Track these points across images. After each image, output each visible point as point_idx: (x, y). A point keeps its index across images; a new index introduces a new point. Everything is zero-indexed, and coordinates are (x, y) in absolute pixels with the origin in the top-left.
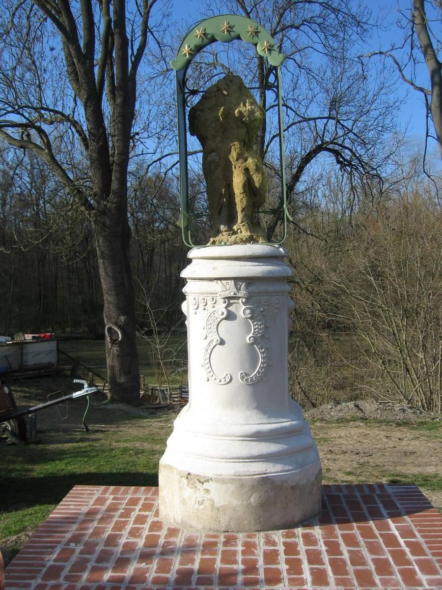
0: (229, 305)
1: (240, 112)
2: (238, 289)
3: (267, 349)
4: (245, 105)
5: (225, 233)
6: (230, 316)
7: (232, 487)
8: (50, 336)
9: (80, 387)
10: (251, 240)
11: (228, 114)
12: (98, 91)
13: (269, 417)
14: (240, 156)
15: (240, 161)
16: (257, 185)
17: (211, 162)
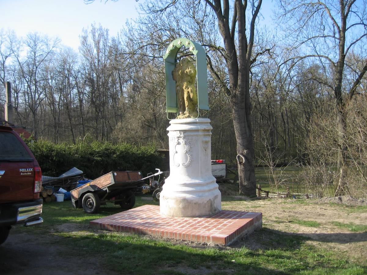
0: (179, 139)
1: (186, 72)
2: (181, 134)
3: (191, 155)
4: (188, 69)
5: (181, 115)
6: (179, 143)
7: (174, 201)
8: (222, 161)
9: (157, 171)
10: (189, 117)
11: (183, 73)
12: (231, 35)
13: (192, 179)
14: (187, 87)
15: (186, 89)
16: (191, 97)
17: (178, 90)
